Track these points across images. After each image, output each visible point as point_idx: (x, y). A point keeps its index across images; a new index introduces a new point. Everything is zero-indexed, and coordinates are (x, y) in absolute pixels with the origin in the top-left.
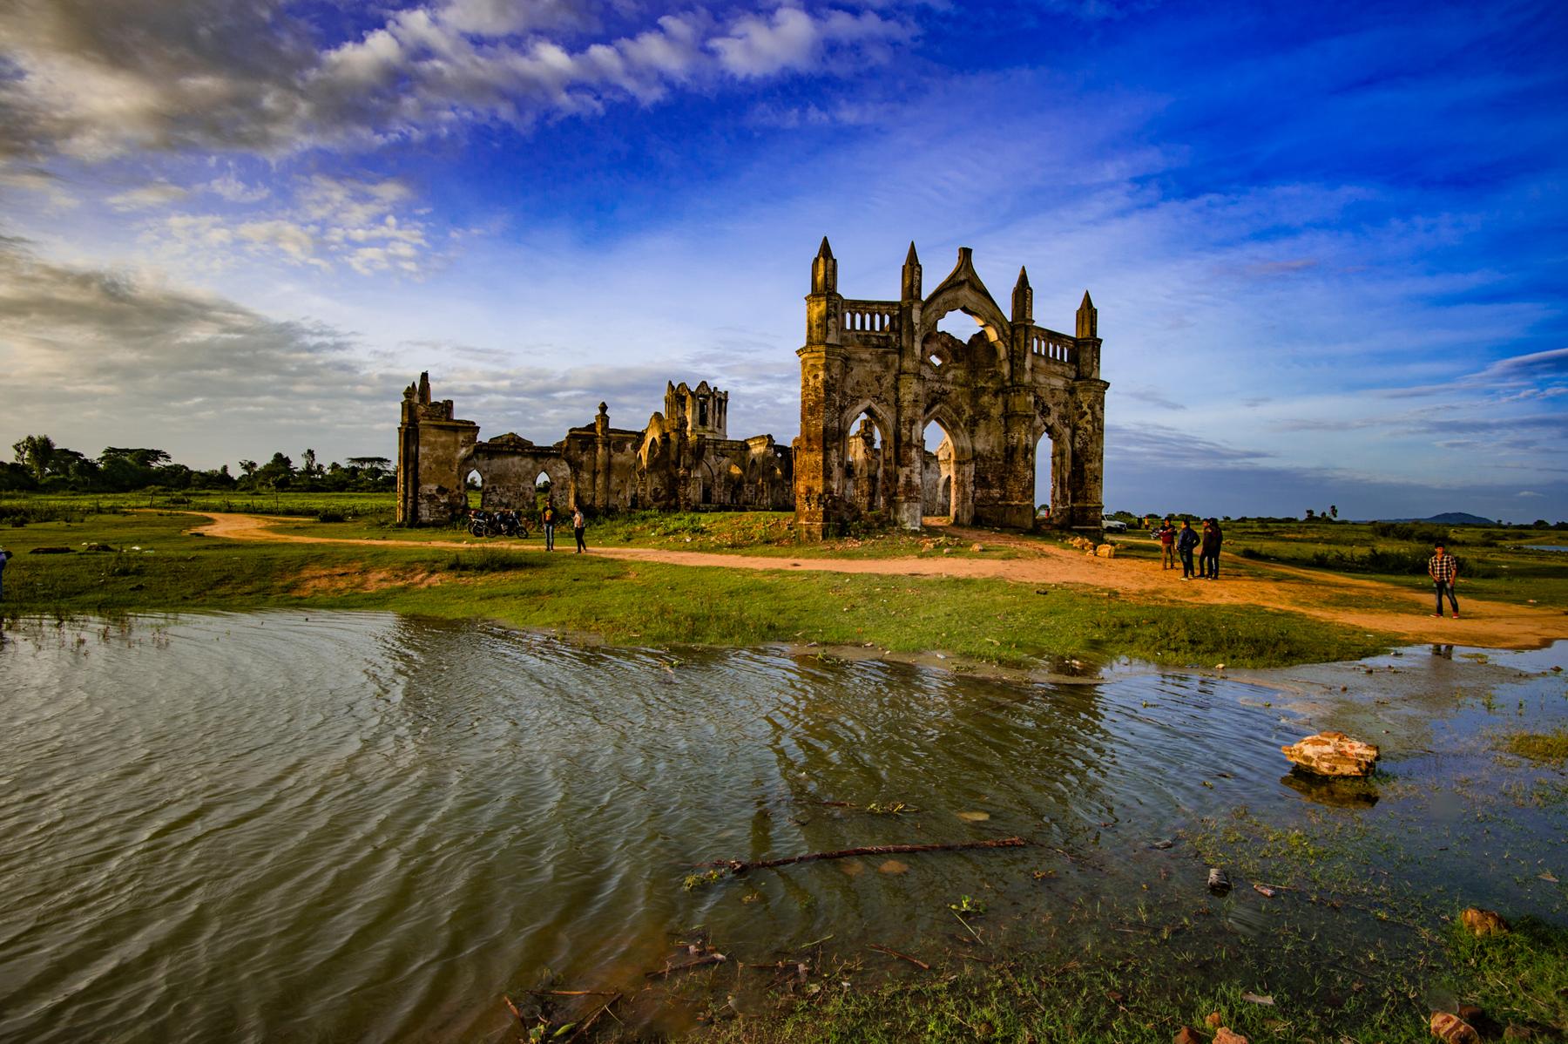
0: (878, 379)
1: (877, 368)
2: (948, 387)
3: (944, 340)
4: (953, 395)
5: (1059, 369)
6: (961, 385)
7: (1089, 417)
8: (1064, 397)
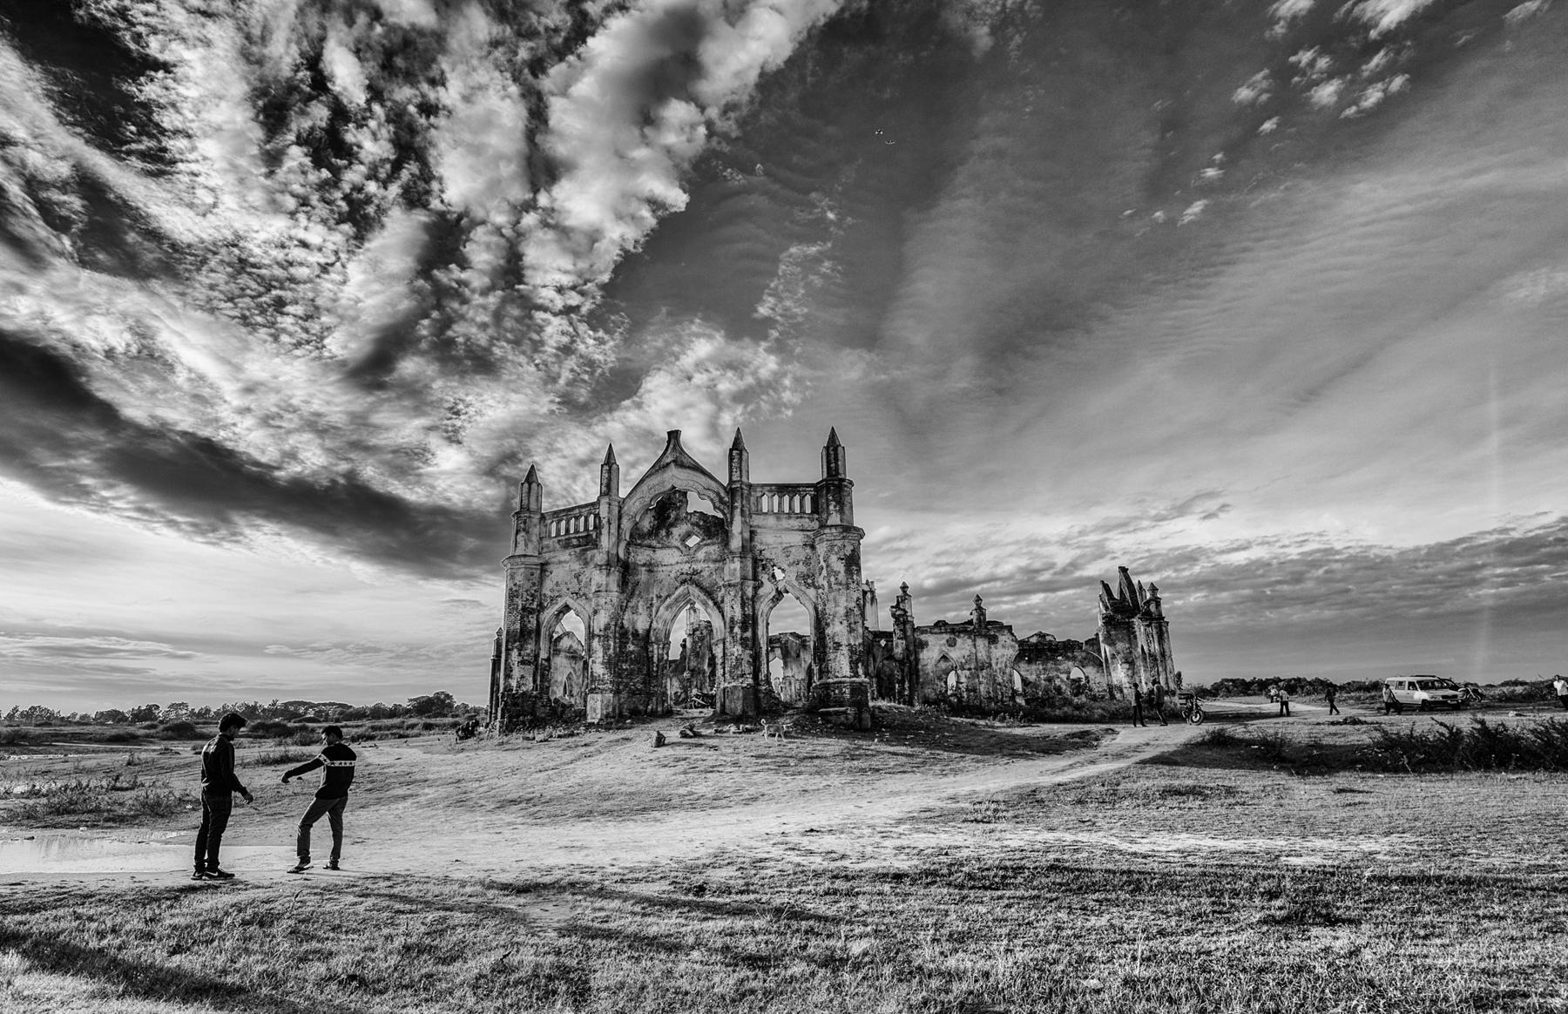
0: (577, 576)
1: (576, 566)
2: (698, 567)
3: (694, 519)
4: (706, 574)
5: (795, 523)
6: (715, 561)
7: (824, 572)
8: (801, 554)
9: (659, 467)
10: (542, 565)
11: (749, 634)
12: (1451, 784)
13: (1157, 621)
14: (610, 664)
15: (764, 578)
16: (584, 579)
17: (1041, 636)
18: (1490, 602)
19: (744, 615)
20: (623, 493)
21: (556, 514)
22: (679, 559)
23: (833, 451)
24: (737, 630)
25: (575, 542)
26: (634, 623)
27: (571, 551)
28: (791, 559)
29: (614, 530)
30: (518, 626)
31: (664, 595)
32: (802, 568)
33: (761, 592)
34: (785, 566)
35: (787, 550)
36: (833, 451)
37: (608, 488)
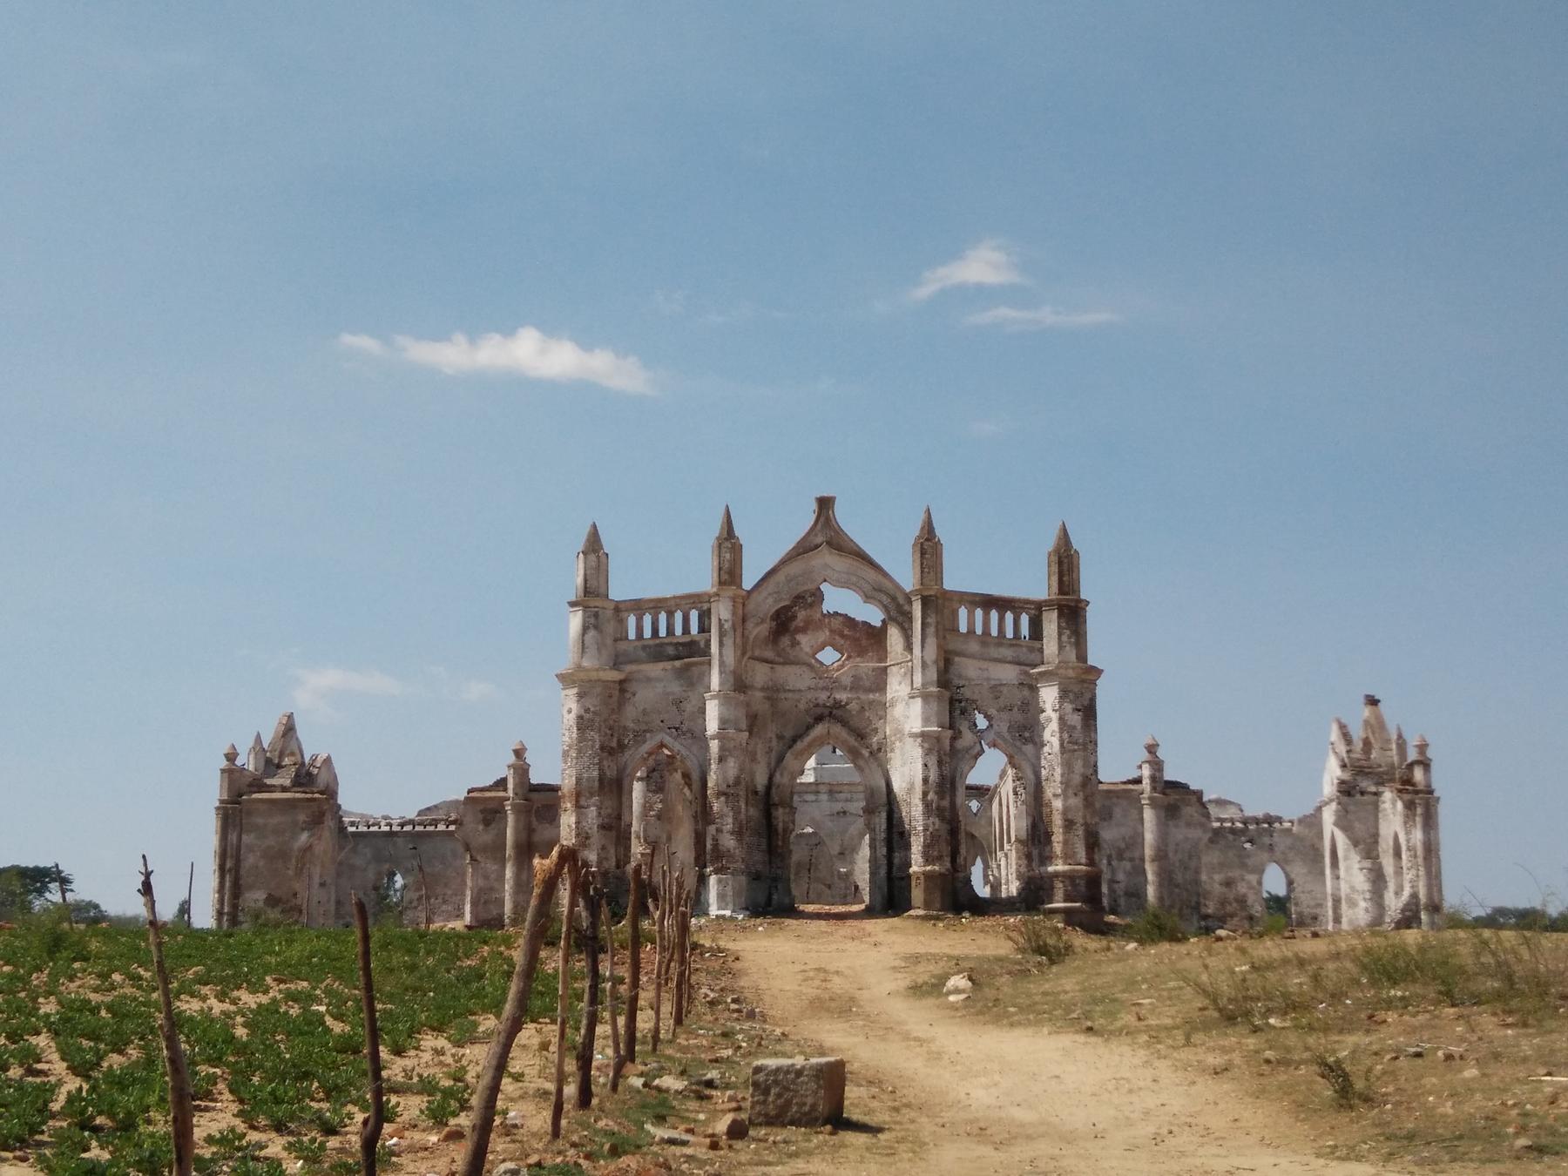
0: (678, 703)
1: (676, 688)
3: (836, 623)
5: (1007, 653)
9: (804, 548)
10: (621, 682)
11: (946, 803)
12: (1162, 1065)
13: (1421, 803)
14: (738, 833)
15: (964, 727)
16: (689, 707)
17: (565, 754)
18: (932, 642)
19: (942, 776)
20: (748, 582)
21: (638, 607)
22: (812, 683)
23: (1065, 562)
24: (931, 796)
25: (671, 651)
26: (752, 775)
27: (668, 665)
28: (1002, 702)
29: (739, 634)
30: (596, 773)
31: (788, 734)
32: (1017, 716)
33: (960, 744)
34: (992, 712)
35: (996, 689)
36: (1065, 562)
37: (729, 574)
